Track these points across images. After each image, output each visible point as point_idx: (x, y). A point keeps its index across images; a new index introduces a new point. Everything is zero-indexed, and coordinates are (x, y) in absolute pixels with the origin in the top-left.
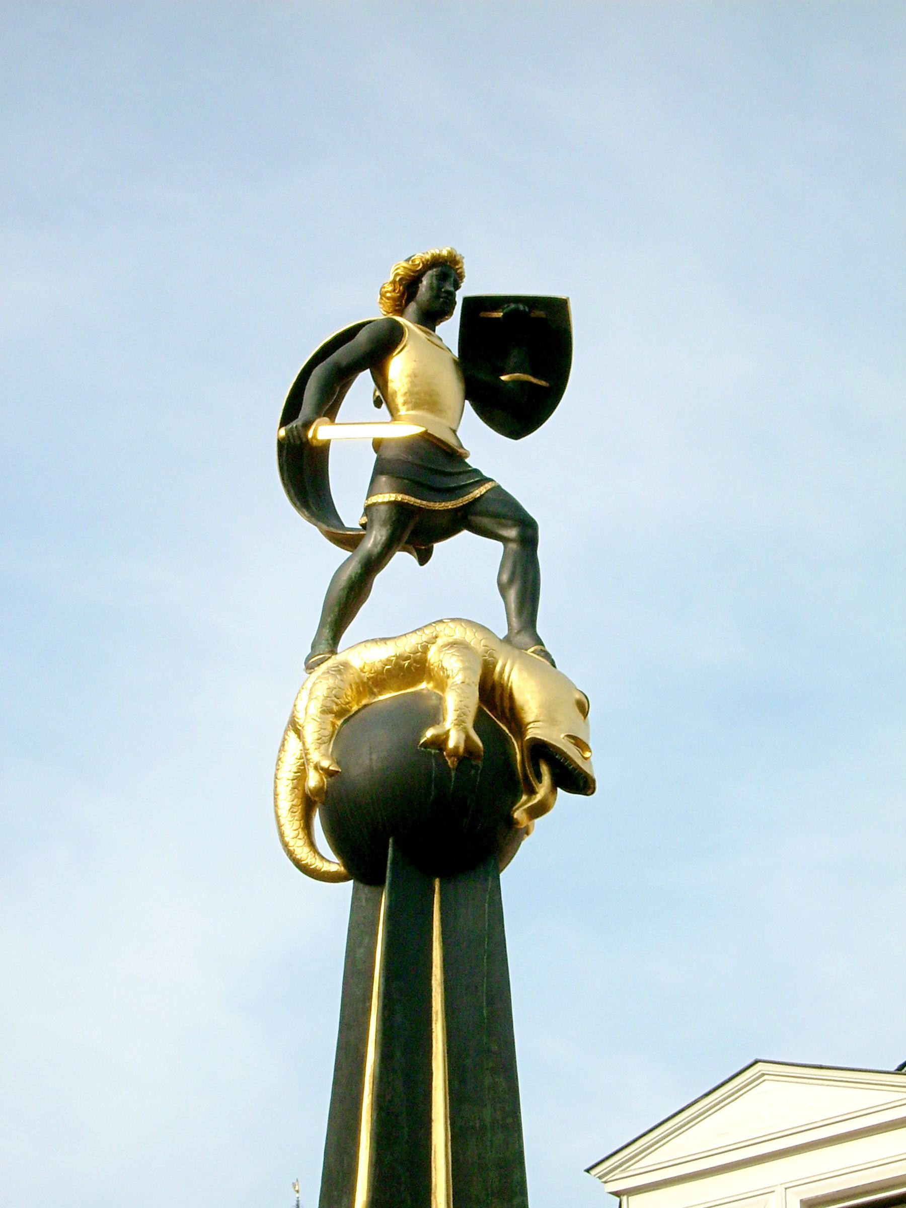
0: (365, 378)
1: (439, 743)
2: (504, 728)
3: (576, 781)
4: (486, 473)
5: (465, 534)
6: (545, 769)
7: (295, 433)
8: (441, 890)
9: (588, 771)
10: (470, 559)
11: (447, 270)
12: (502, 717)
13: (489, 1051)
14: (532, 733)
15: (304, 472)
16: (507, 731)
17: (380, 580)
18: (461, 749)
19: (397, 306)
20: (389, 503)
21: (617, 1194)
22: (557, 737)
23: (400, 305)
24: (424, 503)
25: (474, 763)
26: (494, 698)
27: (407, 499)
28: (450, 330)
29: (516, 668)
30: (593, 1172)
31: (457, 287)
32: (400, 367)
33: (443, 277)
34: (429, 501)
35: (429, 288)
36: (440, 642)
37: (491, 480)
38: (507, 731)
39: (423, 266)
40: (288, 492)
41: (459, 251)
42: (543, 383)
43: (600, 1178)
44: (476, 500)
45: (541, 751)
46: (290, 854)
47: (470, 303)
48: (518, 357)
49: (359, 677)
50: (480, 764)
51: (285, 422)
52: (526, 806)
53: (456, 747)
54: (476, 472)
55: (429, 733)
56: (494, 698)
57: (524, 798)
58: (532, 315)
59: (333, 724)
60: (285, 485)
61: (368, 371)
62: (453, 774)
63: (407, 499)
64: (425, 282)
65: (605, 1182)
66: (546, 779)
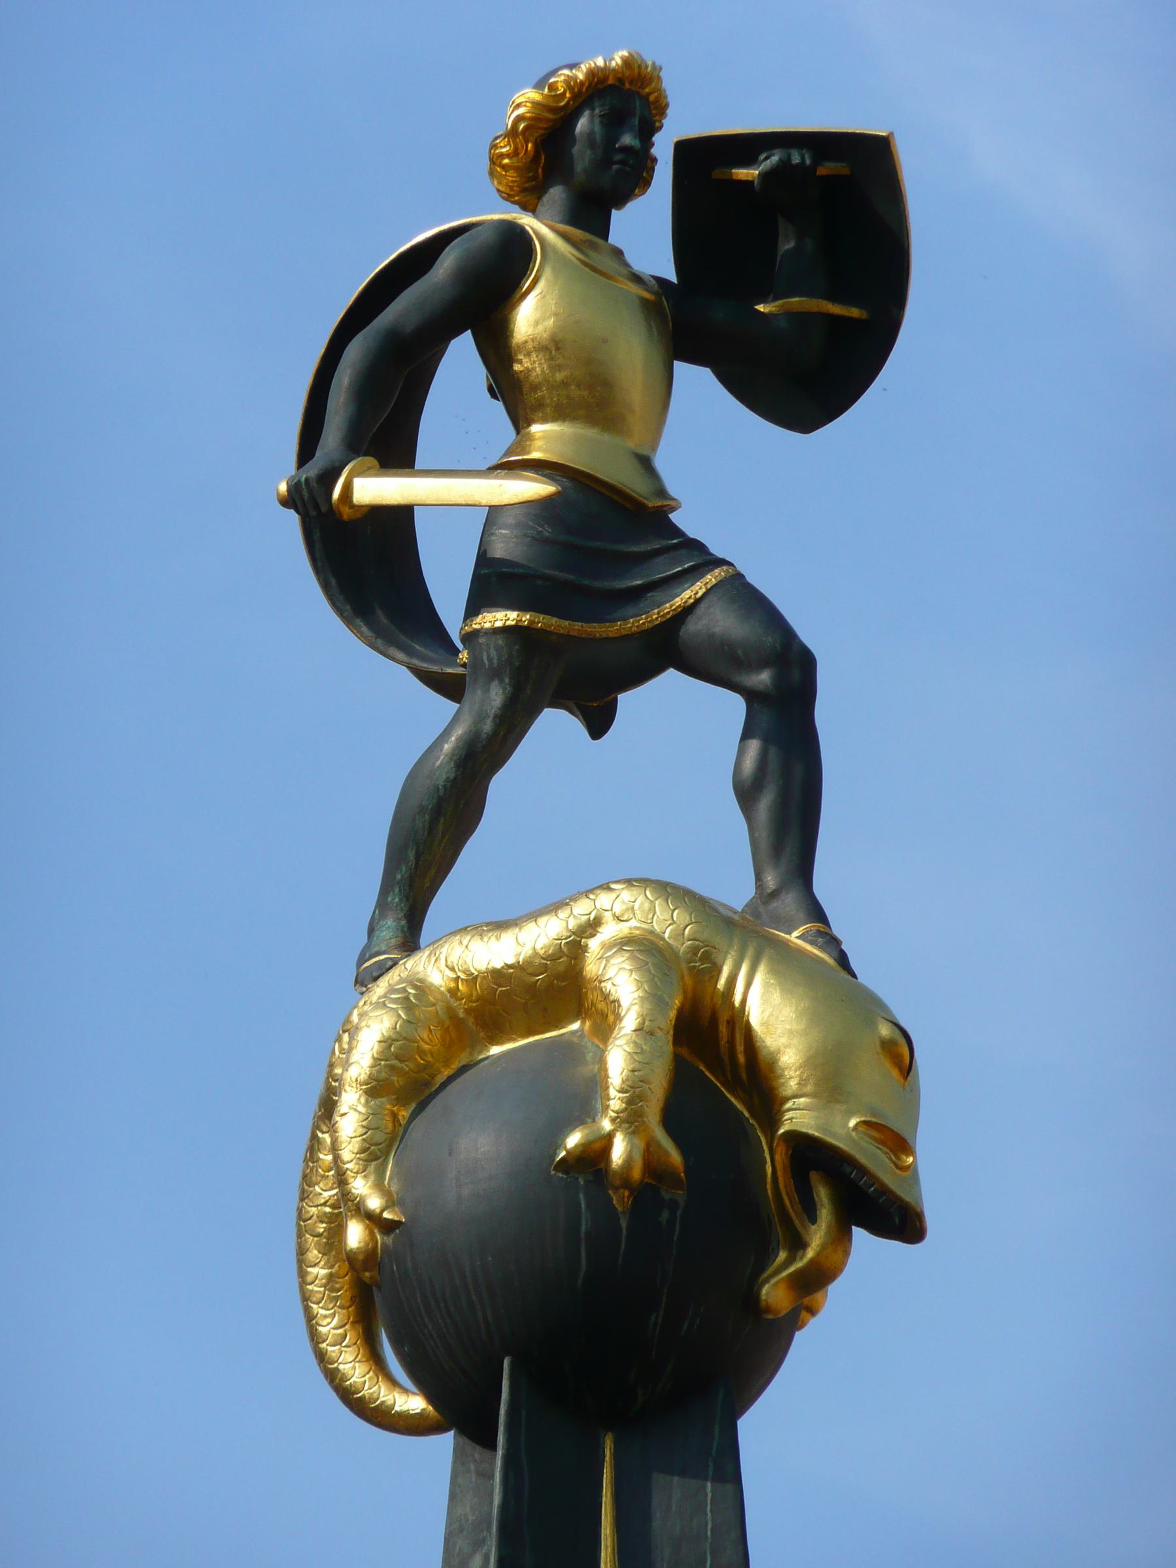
1: (594, 1157)
2: (739, 1106)
5: (672, 675)
6: (822, 1194)
7: (305, 494)
8: (616, 1455)
9: (908, 1198)
10: (685, 725)
11: (626, 99)
12: (734, 1084)
14: (800, 1116)
16: (747, 1114)
17: (502, 787)
18: (637, 1173)
19: (530, 179)
20: (505, 630)
22: (844, 1129)
23: (534, 178)
24: (576, 627)
27: (542, 621)
28: (646, 231)
31: (649, 129)
33: (614, 121)
34: (588, 621)
35: (587, 142)
36: (610, 931)
37: (722, 562)
38: (747, 1114)
39: (575, 96)
41: (649, 57)
42: (855, 312)
45: (808, 1153)
46: (334, 1378)
47: (692, 153)
48: (796, 264)
50: (680, 1195)
52: (784, 1274)
53: (628, 1162)
55: (573, 1140)
57: (782, 1255)
58: (822, 171)
59: (394, 1116)
60: (318, 571)
61: (468, 334)
62: (624, 1224)
63: (542, 621)
64: (582, 124)
66: (825, 1214)
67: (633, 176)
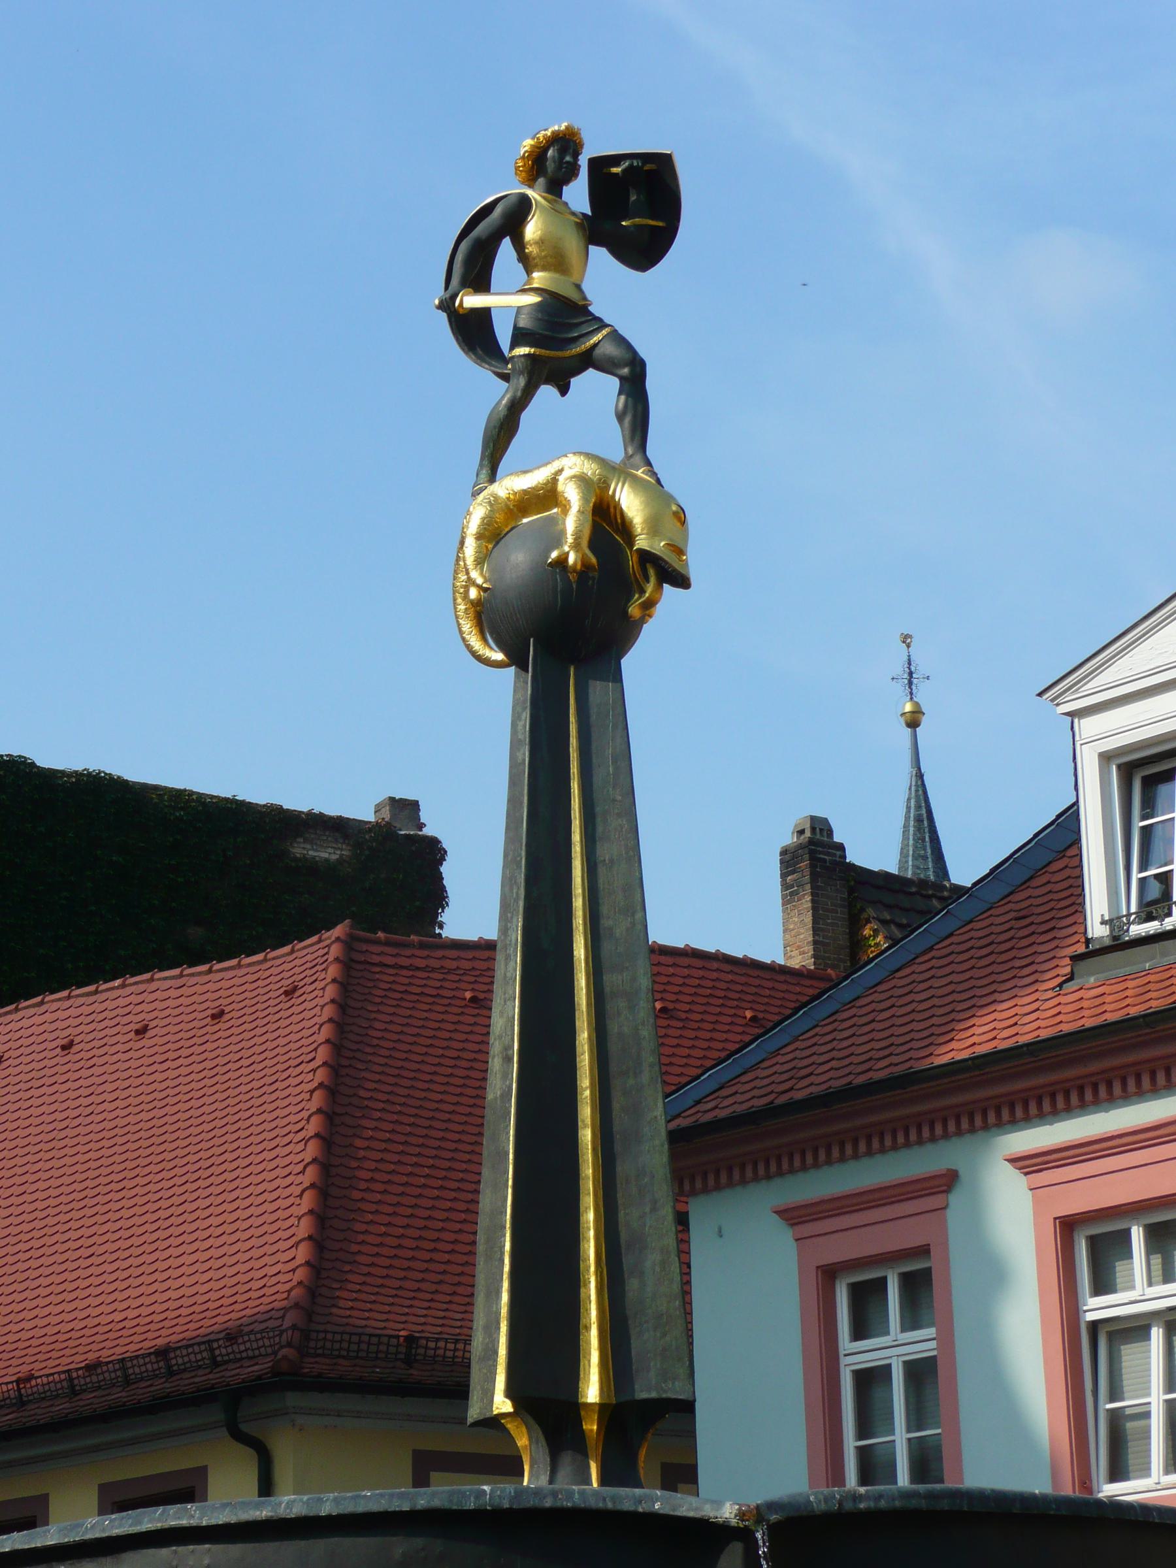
0: (506, 244)
1: (562, 562)
3: (682, 582)
4: (607, 321)
5: (591, 372)
6: (652, 572)
10: (597, 390)
11: (567, 143)
12: (617, 531)
13: (614, 800)
14: (642, 542)
15: (474, 332)
17: (526, 417)
18: (579, 567)
20: (524, 355)
21: (1067, 714)
22: (659, 546)
25: (591, 575)
26: (605, 519)
28: (578, 195)
29: (626, 486)
30: (1045, 697)
32: (532, 230)
33: (562, 152)
35: (553, 161)
40: (457, 340)
42: (661, 224)
43: (1052, 700)
44: (595, 345)
45: (646, 557)
46: (469, 647)
47: (594, 163)
48: (637, 206)
49: (507, 505)
51: (446, 288)
53: (575, 563)
54: (599, 320)
55: (554, 554)
56: (605, 519)
64: (550, 153)
65: (1058, 705)
66: (653, 580)
67: (571, 172)
